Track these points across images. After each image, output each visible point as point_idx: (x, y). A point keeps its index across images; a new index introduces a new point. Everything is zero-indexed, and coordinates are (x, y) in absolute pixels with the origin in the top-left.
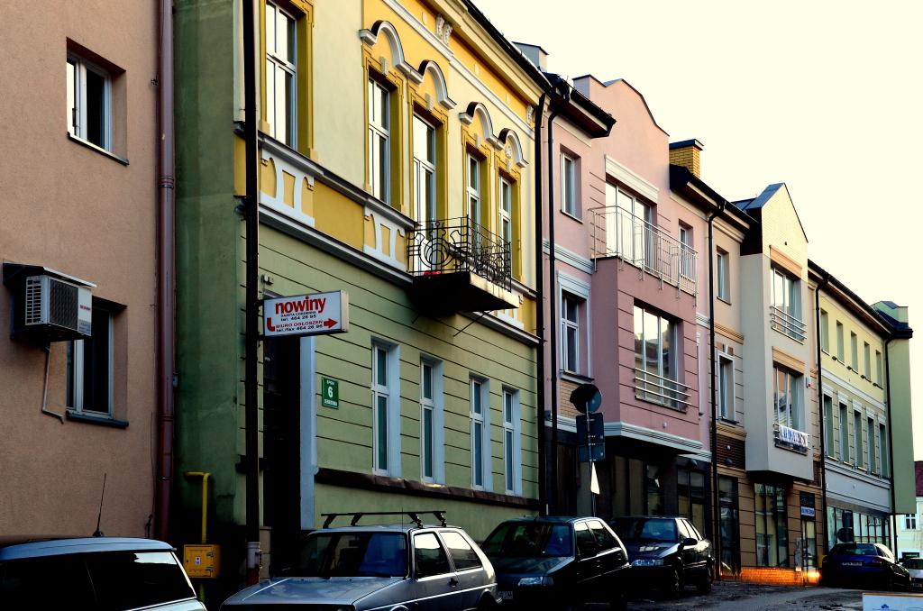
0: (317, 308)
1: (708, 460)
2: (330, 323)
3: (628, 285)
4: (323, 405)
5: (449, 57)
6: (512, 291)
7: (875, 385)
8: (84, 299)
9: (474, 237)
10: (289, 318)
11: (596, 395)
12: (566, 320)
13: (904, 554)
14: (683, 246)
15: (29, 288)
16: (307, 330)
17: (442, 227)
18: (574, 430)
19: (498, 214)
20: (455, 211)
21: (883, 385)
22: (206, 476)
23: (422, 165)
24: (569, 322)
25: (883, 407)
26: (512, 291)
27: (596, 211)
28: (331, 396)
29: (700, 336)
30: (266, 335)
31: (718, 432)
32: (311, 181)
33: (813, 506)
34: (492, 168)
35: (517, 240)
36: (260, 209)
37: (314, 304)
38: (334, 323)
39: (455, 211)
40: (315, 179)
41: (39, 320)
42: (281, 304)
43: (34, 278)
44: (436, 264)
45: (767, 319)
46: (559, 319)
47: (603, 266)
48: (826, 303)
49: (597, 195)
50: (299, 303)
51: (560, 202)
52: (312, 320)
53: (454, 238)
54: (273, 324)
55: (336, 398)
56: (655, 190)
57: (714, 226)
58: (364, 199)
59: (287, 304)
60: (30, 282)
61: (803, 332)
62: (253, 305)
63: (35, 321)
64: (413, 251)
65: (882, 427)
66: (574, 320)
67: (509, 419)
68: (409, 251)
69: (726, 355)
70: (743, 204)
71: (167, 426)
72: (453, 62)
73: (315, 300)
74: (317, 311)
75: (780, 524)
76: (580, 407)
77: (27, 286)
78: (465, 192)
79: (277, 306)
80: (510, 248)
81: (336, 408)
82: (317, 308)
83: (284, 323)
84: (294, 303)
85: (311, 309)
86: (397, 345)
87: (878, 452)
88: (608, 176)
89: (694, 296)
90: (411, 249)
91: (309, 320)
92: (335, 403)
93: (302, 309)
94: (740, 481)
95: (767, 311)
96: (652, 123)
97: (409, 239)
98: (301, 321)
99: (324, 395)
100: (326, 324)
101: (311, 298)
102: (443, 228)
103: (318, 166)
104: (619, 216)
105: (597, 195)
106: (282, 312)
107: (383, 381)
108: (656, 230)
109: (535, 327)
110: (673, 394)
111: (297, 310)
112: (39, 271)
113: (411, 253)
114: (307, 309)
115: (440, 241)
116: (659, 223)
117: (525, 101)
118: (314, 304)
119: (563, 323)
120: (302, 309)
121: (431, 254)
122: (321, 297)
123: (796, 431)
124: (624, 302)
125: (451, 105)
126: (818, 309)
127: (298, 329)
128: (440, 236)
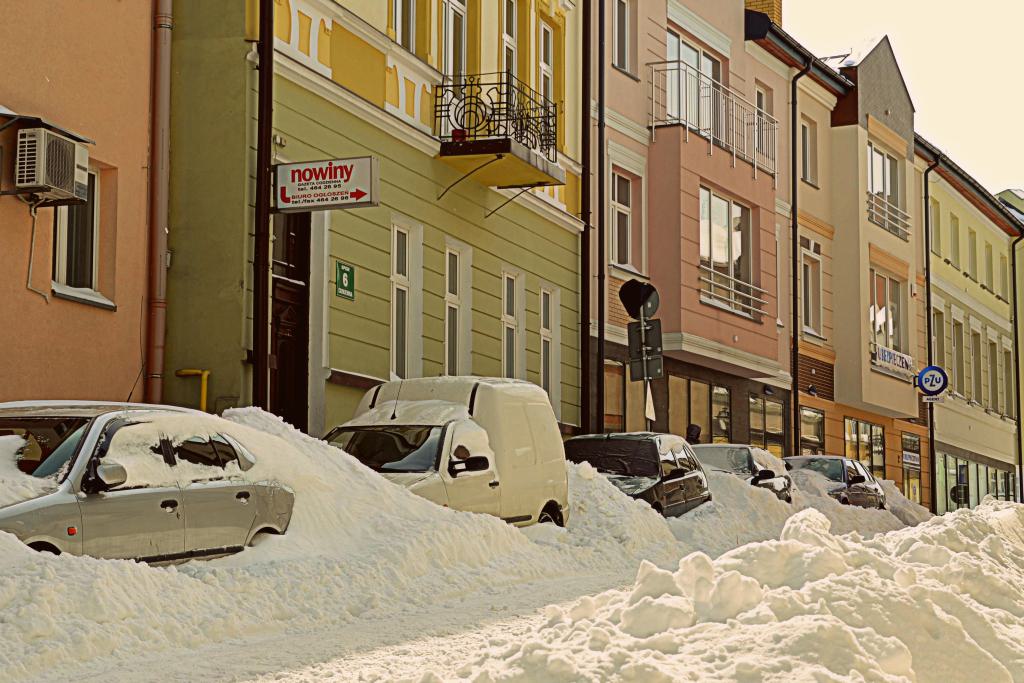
0: (342, 176)
1: (789, 387)
2: (358, 194)
3: (692, 157)
7: (999, 297)
8: (81, 156)
9: (508, 93)
10: (332, 185)
11: (653, 295)
12: (616, 203)
14: (760, 113)
15: (21, 143)
16: (330, 202)
17: (474, 82)
18: (625, 342)
19: (538, 71)
20: (489, 69)
21: (1010, 299)
22: (206, 373)
23: (451, 5)
24: (620, 205)
25: (1009, 327)
27: (654, 66)
28: (346, 285)
29: (781, 230)
30: (279, 207)
31: (800, 351)
33: (918, 452)
34: (533, 11)
35: (559, 105)
37: (339, 171)
38: (363, 194)
39: (489, 69)
41: (34, 180)
42: (299, 171)
43: (27, 131)
45: (863, 207)
46: (608, 203)
47: (665, 133)
48: (938, 186)
49: (656, 47)
51: (611, 56)
52: (337, 190)
53: (489, 96)
54: (288, 195)
55: (351, 288)
56: (728, 39)
57: (800, 89)
59: (305, 170)
60: (23, 136)
61: (906, 226)
62: (265, 171)
63: (28, 181)
64: (441, 111)
65: (1007, 353)
66: (627, 205)
67: (547, 326)
68: (436, 111)
69: (811, 253)
71: (160, 313)
73: (340, 167)
74: (342, 180)
76: (633, 312)
77: (19, 140)
78: (500, 40)
79: (293, 172)
80: (551, 115)
81: (352, 299)
82: (342, 176)
83: (302, 193)
84: (315, 169)
85: (336, 177)
87: (1001, 386)
88: (668, 19)
89: (773, 176)
90: (439, 108)
91: (332, 190)
92: (349, 294)
93: (324, 177)
95: (863, 198)
96: (515, 184)
97: (437, 97)
98: (323, 191)
99: (339, 284)
100: (353, 195)
101: (336, 164)
102: (478, 85)
104: (682, 73)
105: (656, 47)
106: (300, 180)
107: (402, 270)
108: (727, 93)
109: (580, 211)
110: (747, 301)
111: (317, 178)
112: (36, 123)
113: (438, 114)
114: (330, 178)
115: (474, 100)
116: (731, 83)
118: (339, 171)
119: (613, 207)
120: (324, 177)
121: (463, 116)
122: (348, 164)
123: (897, 353)
124: (687, 181)
126: (926, 197)
127: (319, 200)
128: (474, 94)
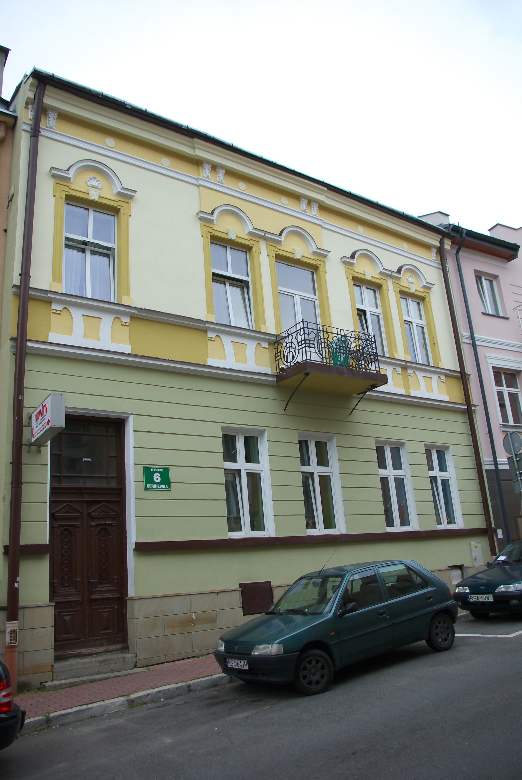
4: (146, 489)
5: (321, 224)
32: (443, 378)
40: (401, 368)
44: (290, 362)
58: (204, 326)
72: (325, 226)
81: (168, 489)
86: (450, 446)
92: (165, 486)
103: (444, 369)
117: (427, 247)
125: (431, 286)
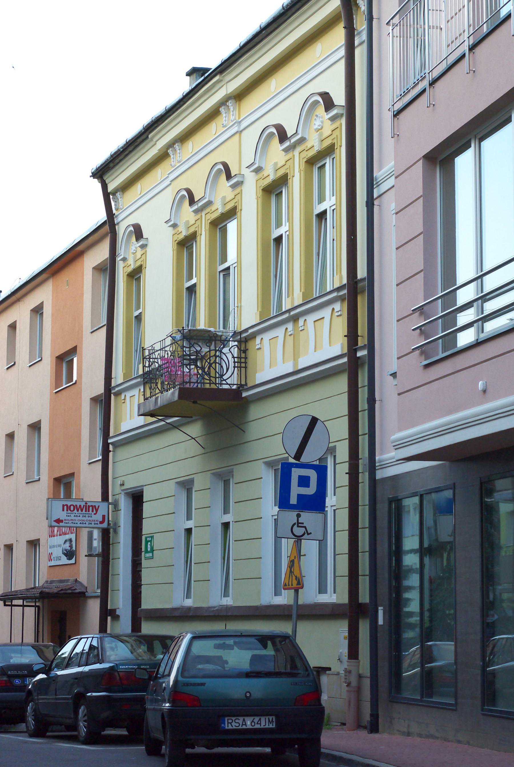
0: (93, 511)
6: (247, 348)
10: (72, 515)
13: (335, 447)
26: (247, 348)
36: (323, 750)
37: (91, 508)
42: (67, 505)
50: (80, 506)
52: (90, 518)
70: (294, 547)
73: (92, 506)
74: (93, 513)
75: (262, 675)
79: (63, 506)
82: (93, 511)
84: (76, 505)
85: (89, 511)
93: (82, 511)
94: (154, 361)
106: (67, 510)
111: (78, 511)
114: (86, 511)
118: (91, 508)
120: (82, 511)
127: (81, 523)
